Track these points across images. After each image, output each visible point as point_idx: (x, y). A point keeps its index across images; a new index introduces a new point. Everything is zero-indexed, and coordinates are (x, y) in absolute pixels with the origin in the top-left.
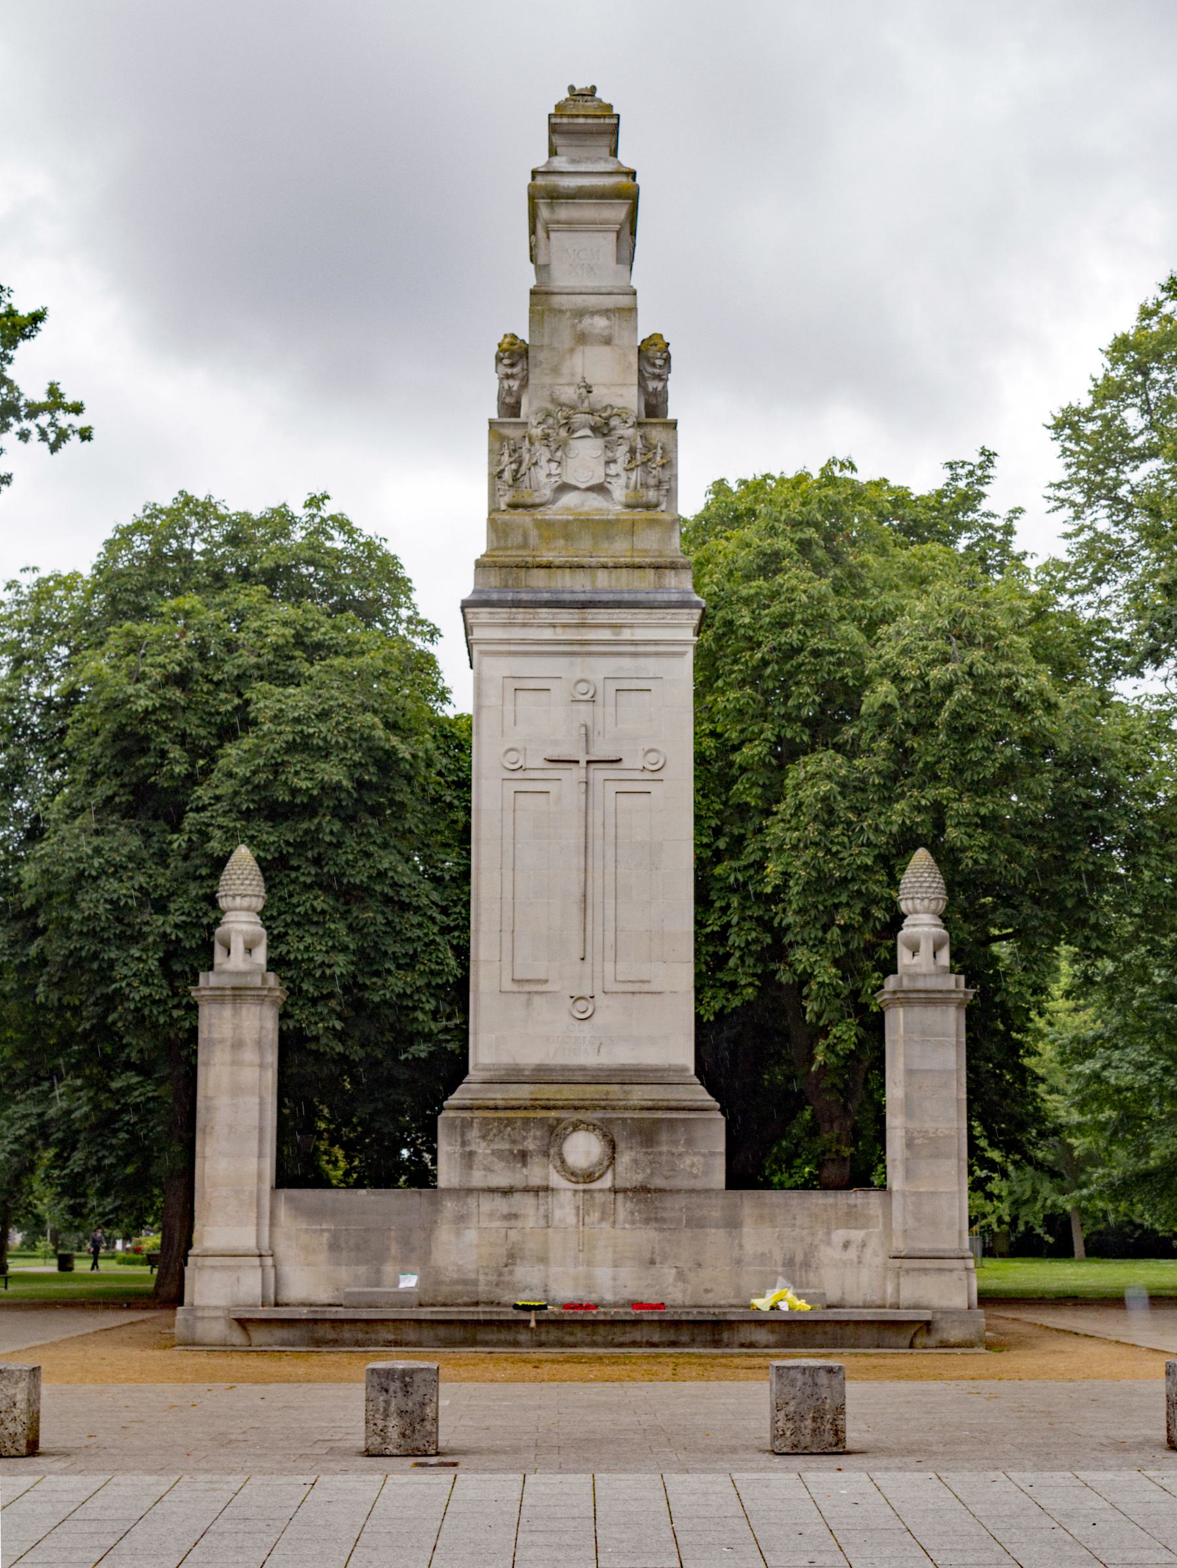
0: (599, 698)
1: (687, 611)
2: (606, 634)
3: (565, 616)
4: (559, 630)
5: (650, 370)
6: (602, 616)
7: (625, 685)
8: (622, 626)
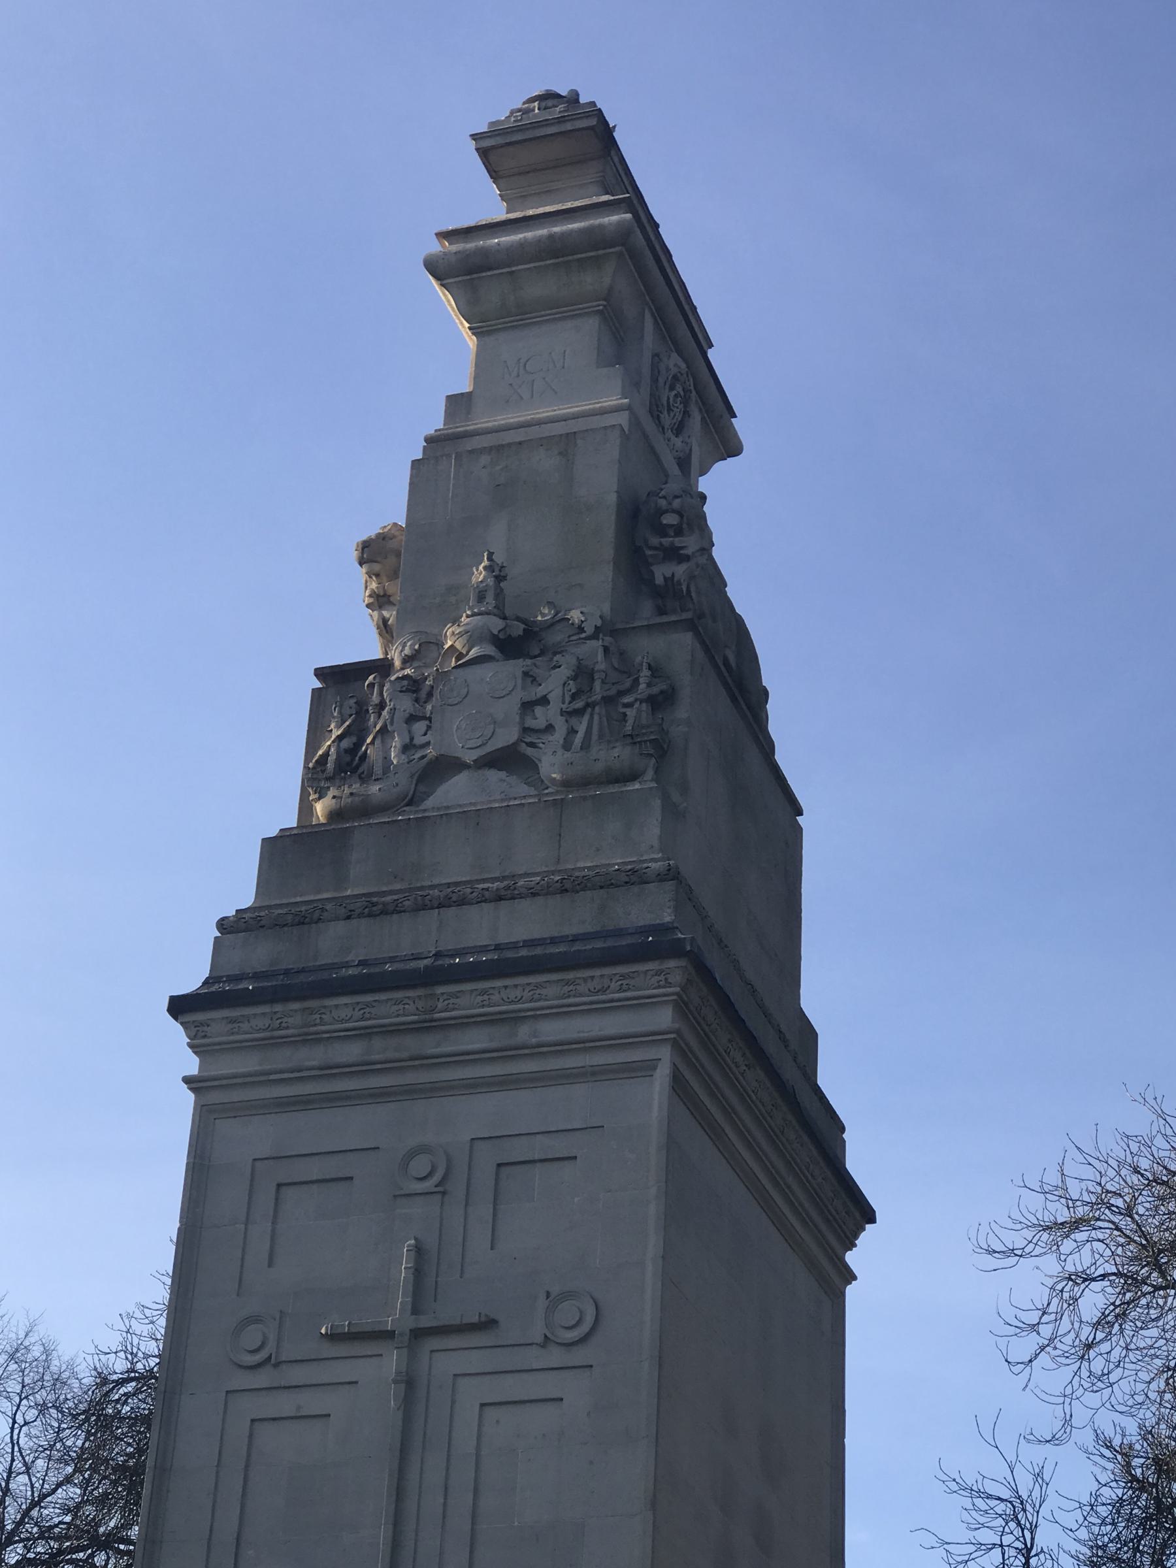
1: (652, 966)
2: (475, 1040)
3: (390, 1007)
4: (377, 1043)
5: (655, 541)
6: (466, 998)
7: (519, 1150)
8: (513, 1019)
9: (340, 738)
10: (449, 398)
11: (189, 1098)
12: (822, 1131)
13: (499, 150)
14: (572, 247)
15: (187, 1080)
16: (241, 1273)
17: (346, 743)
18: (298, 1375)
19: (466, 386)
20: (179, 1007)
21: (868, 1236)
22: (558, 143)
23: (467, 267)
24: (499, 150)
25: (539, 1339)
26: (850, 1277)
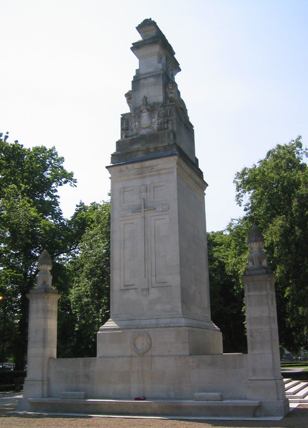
0: (148, 190)
9: (125, 125)
10: (137, 28)
11: (110, 180)
12: (200, 174)
13: (140, 28)
14: (152, 40)
15: (110, 178)
16: (131, 289)
17: (126, 126)
18: (130, 217)
19: (138, 68)
20: (107, 167)
21: (208, 188)
22: (148, 26)
23: (136, 47)
24: (140, 28)
25: (161, 210)
26: (205, 194)
